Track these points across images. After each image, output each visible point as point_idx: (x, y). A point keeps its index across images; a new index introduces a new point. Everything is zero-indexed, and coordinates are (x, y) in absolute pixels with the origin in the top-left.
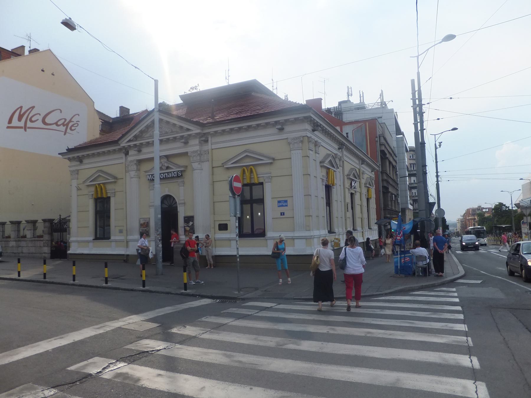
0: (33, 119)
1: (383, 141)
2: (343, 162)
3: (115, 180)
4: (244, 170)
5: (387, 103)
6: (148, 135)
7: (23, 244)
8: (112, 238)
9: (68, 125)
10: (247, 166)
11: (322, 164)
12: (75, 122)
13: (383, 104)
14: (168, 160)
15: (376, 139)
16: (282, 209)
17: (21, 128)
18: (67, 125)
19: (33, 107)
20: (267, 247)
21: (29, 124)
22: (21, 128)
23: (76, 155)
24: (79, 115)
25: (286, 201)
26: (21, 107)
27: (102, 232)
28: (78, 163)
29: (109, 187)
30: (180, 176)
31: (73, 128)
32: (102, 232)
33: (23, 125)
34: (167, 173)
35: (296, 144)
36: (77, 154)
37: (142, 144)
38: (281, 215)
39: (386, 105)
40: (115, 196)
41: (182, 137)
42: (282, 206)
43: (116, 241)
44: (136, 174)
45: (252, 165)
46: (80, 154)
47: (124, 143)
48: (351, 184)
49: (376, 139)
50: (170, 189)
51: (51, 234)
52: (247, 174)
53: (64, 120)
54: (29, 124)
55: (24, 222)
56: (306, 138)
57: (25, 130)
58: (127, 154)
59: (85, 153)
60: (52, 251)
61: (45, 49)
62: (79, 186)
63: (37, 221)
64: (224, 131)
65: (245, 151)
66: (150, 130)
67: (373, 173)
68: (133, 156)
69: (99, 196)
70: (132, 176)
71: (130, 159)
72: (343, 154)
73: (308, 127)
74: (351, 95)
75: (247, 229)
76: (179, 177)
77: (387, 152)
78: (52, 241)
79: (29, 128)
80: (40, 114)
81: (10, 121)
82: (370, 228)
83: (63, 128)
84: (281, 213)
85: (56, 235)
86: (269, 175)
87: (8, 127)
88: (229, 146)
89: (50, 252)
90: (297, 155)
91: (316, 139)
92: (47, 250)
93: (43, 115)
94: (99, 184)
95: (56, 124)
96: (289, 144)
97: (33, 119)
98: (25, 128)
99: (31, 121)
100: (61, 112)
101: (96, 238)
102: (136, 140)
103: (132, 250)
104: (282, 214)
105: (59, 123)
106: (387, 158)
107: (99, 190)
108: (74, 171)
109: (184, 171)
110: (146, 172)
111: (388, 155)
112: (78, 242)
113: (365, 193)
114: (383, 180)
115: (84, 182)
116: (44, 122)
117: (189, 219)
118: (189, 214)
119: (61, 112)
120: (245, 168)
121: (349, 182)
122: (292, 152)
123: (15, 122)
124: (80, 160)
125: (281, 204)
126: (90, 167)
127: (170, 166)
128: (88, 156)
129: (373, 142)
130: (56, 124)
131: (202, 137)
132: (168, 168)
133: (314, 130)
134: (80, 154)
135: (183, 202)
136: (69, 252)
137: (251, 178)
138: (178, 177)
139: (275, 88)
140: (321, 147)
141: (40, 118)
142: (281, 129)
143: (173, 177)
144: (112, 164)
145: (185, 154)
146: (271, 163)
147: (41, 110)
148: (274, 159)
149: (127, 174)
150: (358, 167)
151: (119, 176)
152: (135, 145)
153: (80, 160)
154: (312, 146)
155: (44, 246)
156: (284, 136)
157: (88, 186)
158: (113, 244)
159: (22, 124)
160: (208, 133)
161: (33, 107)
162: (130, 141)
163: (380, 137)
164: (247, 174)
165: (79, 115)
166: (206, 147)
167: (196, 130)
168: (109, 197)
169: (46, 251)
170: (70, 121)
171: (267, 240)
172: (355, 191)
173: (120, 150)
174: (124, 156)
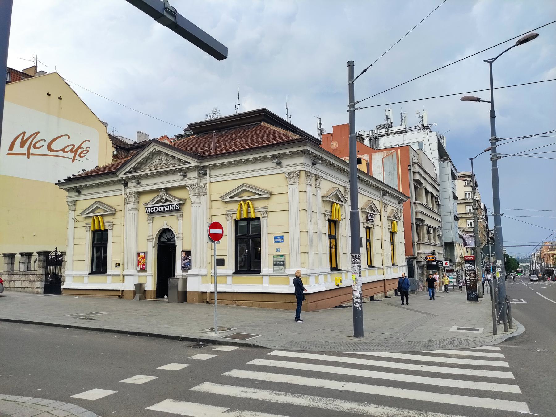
0: (37, 145)
3: (114, 213)
4: (241, 204)
6: (147, 167)
8: (108, 272)
9: (77, 152)
14: (167, 193)
17: (24, 154)
18: (76, 151)
21: (33, 151)
22: (24, 154)
23: (73, 186)
24: (89, 141)
25: (282, 237)
27: (99, 265)
28: (76, 194)
29: (107, 219)
30: (178, 209)
31: (82, 155)
32: (99, 265)
33: (26, 152)
34: (166, 206)
35: (292, 179)
36: (74, 184)
37: (140, 175)
41: (181, 170)
42: (279, 242)
43: (112, 276)
45: (250, 200)
46: (78, 185)
47: (122, 175)
50: (161, 223)
52: (245, 208)
53: (72, 146)
54: (33, 151)
55: (35, 254)
57: (28, 157)
58: (126, 185)
59: (83, 184)
60: (45, 285)
61: (51, 72)
62: (76, 217)
63: (33, 253)
64: (230, 163)
65: (243, 186)
66: (148, 162)
68: (132, 187)
70: (131, 209)
71: (128, 190)
73: (308, 162)
76: (178, 210)
78: (47, 274)
79: (32, 154)
80: (45, 141)
81: (11, 148)
82: (370, 266)
83: (71, 155)
84: (280, 249)
85: (51, 269)
86: (266, 210)
87: (9, 154)
88: (225, 180)
89: (43, 286)
91: (316, 172)
92: (40, 284)
93: (48, 141)
95: (64, 150)
96: (287, 178)
97: (37, 145)
98: (28, 155)
99: (35, 147)
100: (69, 138)
101: (92, 273)
102: (135, 172)
103: (129, 285)
105: (66, 150)
108: (72, 202)
109: (183, 204)
110: (144, 204)
111: (425, 184)
113: (387, 226)
115: (81, 214)
119: (69, 138)
120: (242, 202)
123: (17, 148)
124: (78, 191)
126: (86, 200)
127: (168, 199)
128: (87, 187)
130: (64, 150)
132: (167, 201)
134: (78, 185)
135: (181, 236)
136: (62, 287)
137: (248, 213)
138: (176, 210)
139: (289, 116)
140: (323, 181)
141: (45, 144)
143: (171, 211)
144: (113, 196)
145: (184, 187)
146: (268, 198)
147: (46, 135)
148: (271, 194)
149: (126, 206)
151: (118, 208)
152: (134, 177)
153: (78, 191)
154: (312, 181)
155: (37, 280)
156: (282, 170)
157: (86, 218)
159: (25, 150)
160: (207, 167)
162: (128, 172)
164: (245, 208)
165: (89, 141)
166: (207, 180)
167: (194, 163)
168: (107, 230)
169: (39, 286)
170: (79, 147)
171: (262, 276)
173: (120, 181)
174: (122, 187)
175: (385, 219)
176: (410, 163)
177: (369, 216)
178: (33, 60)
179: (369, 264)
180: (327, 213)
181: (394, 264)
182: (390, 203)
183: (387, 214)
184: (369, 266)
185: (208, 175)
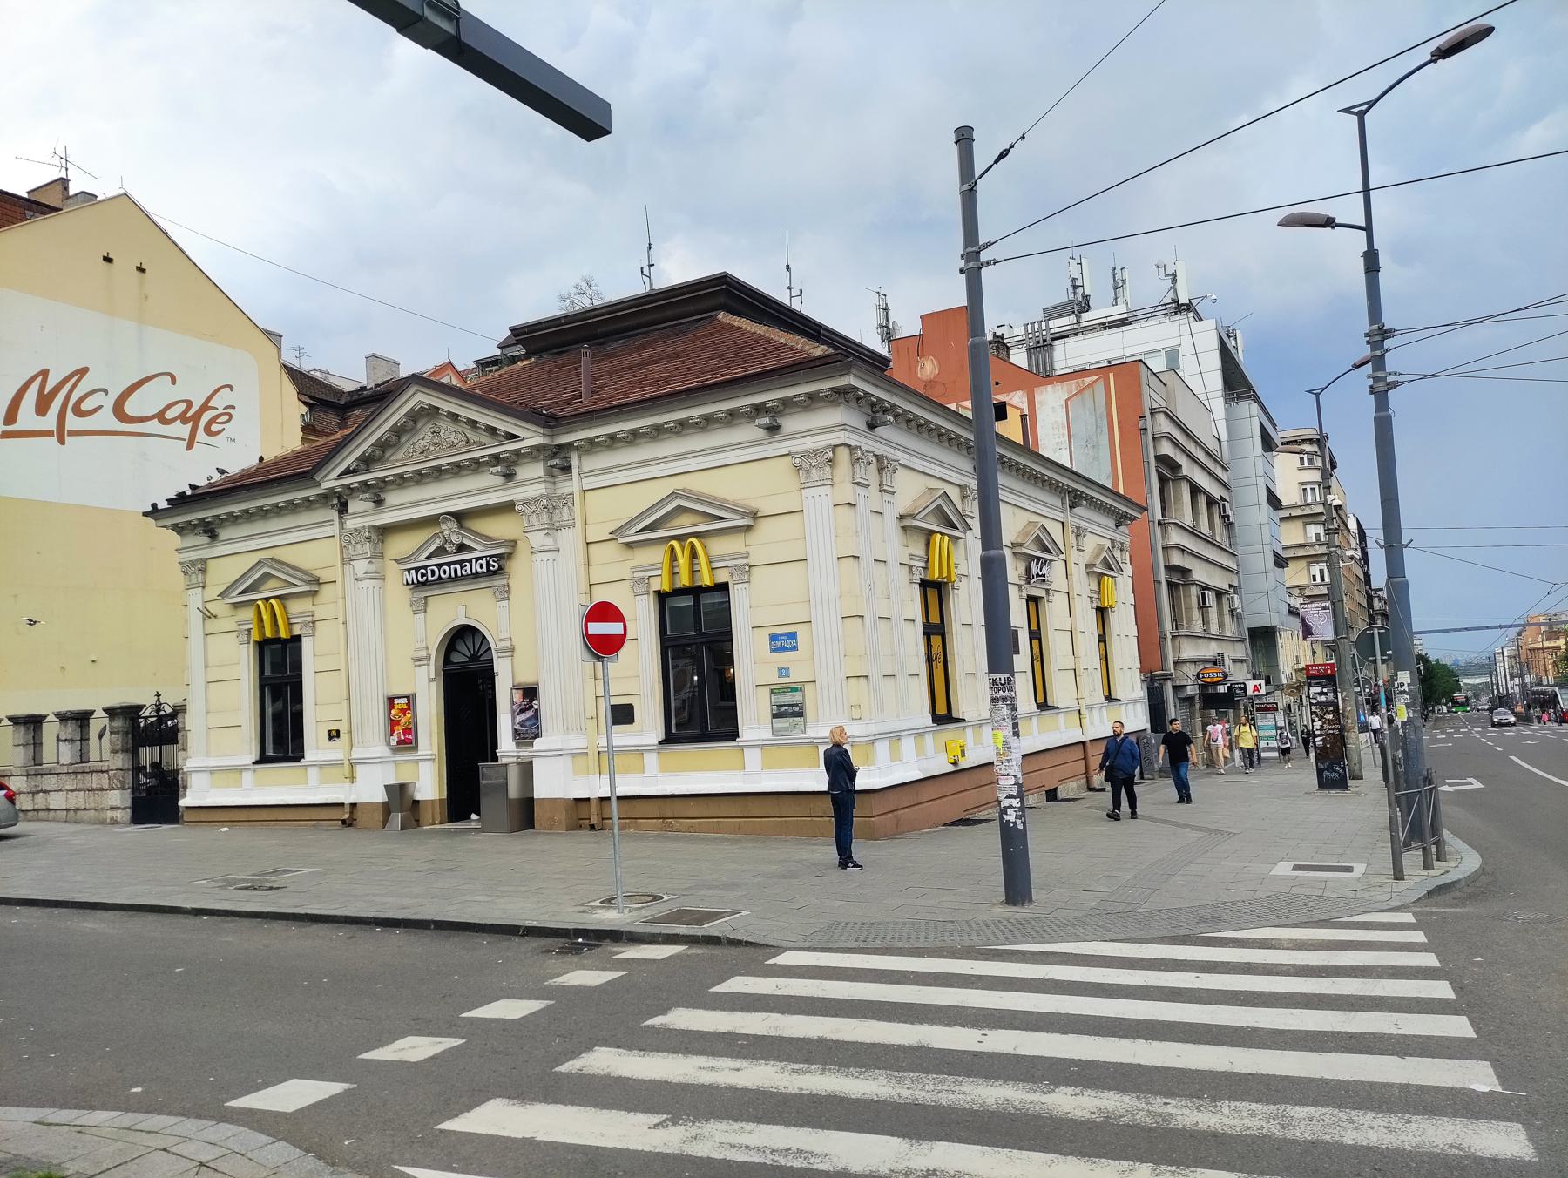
0: (85, 406)
4: (673, 549)
6: (400, 455)
7: (50, 782)
8: (309, 754)
9: (198, 419)
10: (681, 538)
11: (907, 523)
12: (221, 411)
14: (461, 527)
16: (784, 658)
17: (48, 433)
19: (83, 372)
21: (72, 422)
22: (48, 433)
24: (231, 388)
25: (793, 636)
26: (45, 373)
27: (282, 737)
29: (295, 607)
30: (496, 570)
31: (215, 428)
32: (282, 737)
33: (53, 427)
34: (460, 562)
36: (198, 511)
37: (382, 480)
40: (313, 635)
41: (496, 459)
42: (783, 649)
43: (321, 766)
45: (697, 535)
46: (208, 514)
47: (330, 481)
51: (135, 753)
52: (683, 560)
54: (72, 422)
55: (100, 713)
57: (62, 441)
58: (343, 509)
59: (222, 511)
62: (209, 606)
63: (92, 712)
68: (363, 515)
69: (684, 580)
70: (361, 575)
71: (352, 523)
73: (856, 419)
76: (495, 573)
78: (137, 769)
79: (72, 433)
80: (106, 392)
81: (11, 417)
82: (1043, 706)
83: (183, 430)
85: (147, 755)
86: (744, 561)
89: (129, 803)
92: (119, 799)
93: (114, 394)
94: (267, 599)
95: (160, 417)
96: (798, 468)
97: (85, 406)
98: (61, 434)
99: (79, 413)
100: (174, 381)
101: (263, 759)
102: (367, 470)
103: (369, 790)
105: (169, 415)
107: (266, 616)
108: (193, 563)
109: (509, 556)
112: (212, 771)
113: (1086, 593)
116: (119, 411)
118: (526, 678)
119: (174, 381)
120: (674, 543)
123: (27, 418)
124: (210, 530)
127: (466, 541)
128: (233, 519)
130: (160, 417)
131: (552, 457)
132: (462, 548)
133: (872, 427)
134: (208, 514)
135: (507, 644)
136: (182, 803)
138: (491, 573)
139: (795, 292)
140: (901, 472)
141: (108, 402)
142: (773, 429)
143: (476, 575)
145: (507, 508)
146: (748, 528)
147: (109, 377)
148: (755, 516)
151: (324, 575)
152: (365, 486)
155: (111, 788)
156: (783, 447)
157: (236, 605)
158: (313, 773)
159: (49, 422)
160: (569, 446)
161: (83, 372)
162: (348, 472)
164: (683, 560)
166: (572, 485)
167: (531, 437)
168: (298, 638)
169: (118, 803)
170: (206, 407)
173: (325, 498)
174: (334, 514)
175: (1078, 573)
177: (1033, 564)
178: (57, 161)
179: (1041, 700)
181: (1109, 698)
182: (1091, 527)
183: (1085, 557)
184: (1039, 706)
185: (575, 471)
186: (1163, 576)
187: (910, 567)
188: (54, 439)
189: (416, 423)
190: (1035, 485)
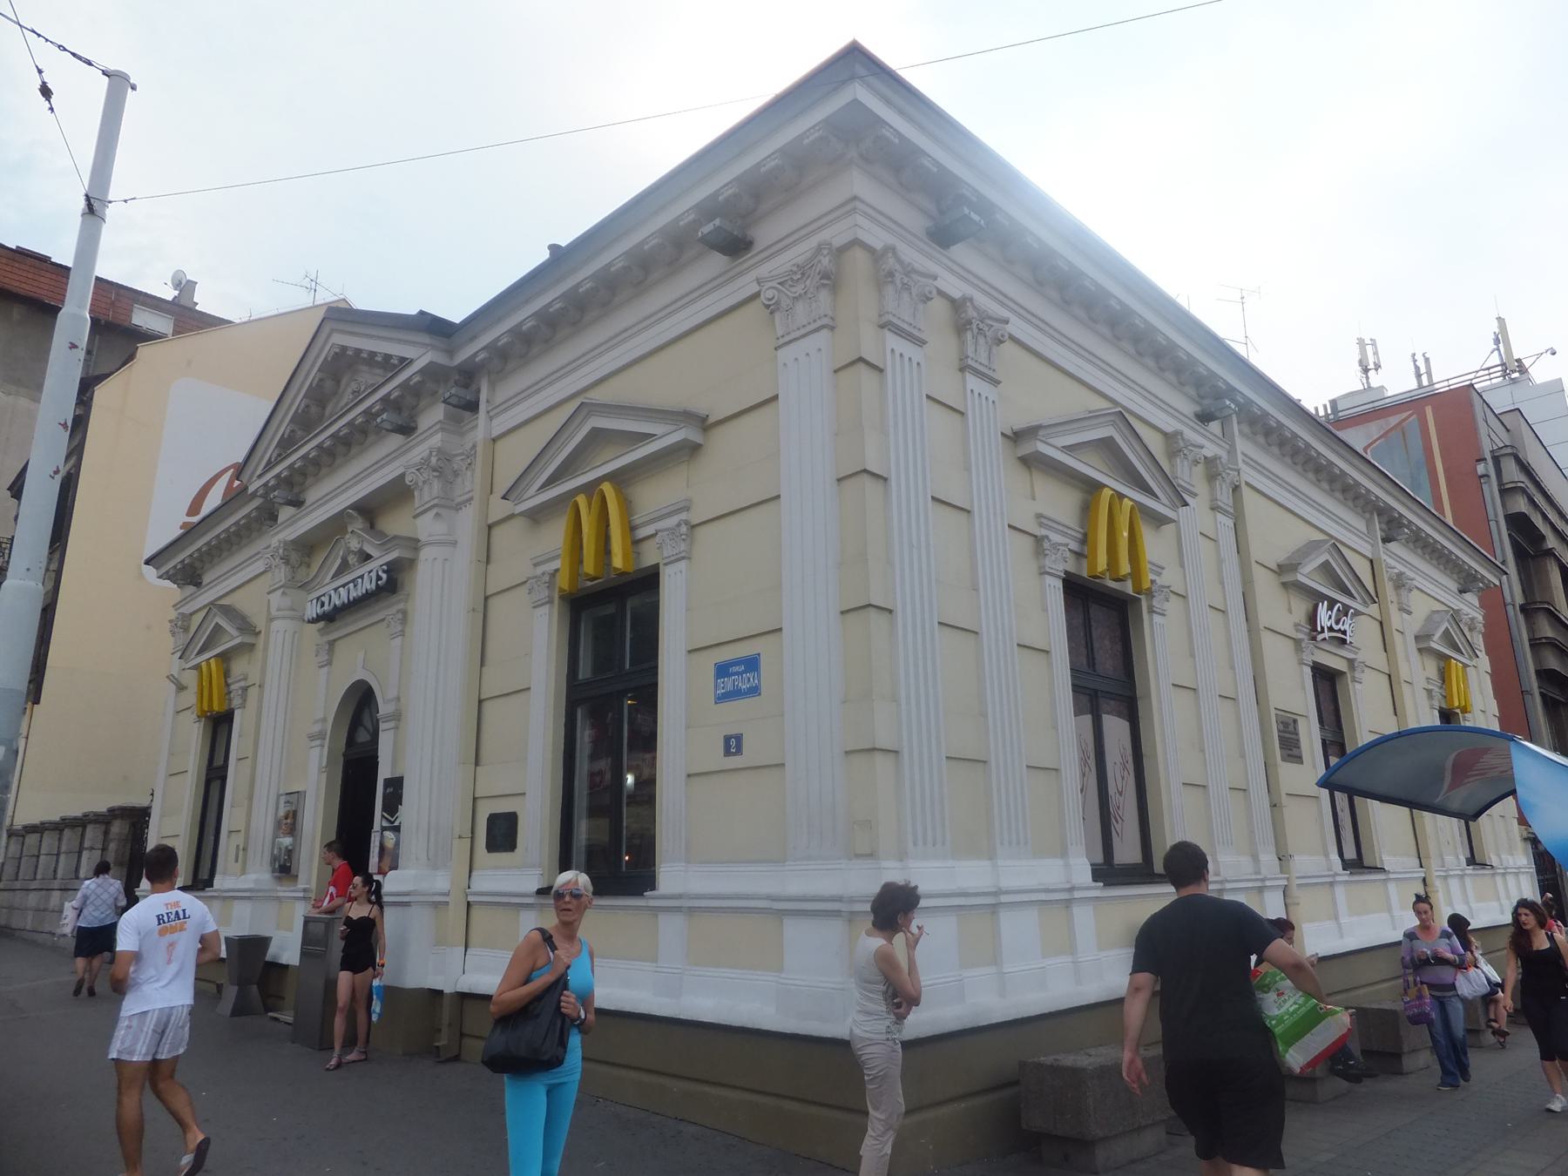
1: (1512, 473)
2: (1236, 489)
5: (1527, 363)
8: (671, 876)
13: (1514, 370)
15: (1481, 469)
16: (735, 716)
20: (654, 959)
25: (752, 664)
38: (727, 753)
39: (1522, 369)
42: (735, 694)
44: (287, 602)
48: (1312, 618)
49: (1481, 469)
56: (859, 255)
67: (1468, 596)
72: (1232, 451)
74: (1377, 367)
75: (1127, 851)
77: (1538, 521)
84: (727, 739)
86: (683, 516)
90: (804, 373)
104: (733, 745)
106: (1550, 553)
113: (1420, 683)
114: (1536, 644)
117: (395, 785)
121: (1300, 608)
122: (786, 354)
125: (729, 683)
129: (1464, 484)
148: (705, 424)
150: (1366, 549)
162: (270, 465)
163: (1497, 461)
172: (1351, 662)
175: (1405, 647)
176: (1479, 448)
177: (1323, 609)
178: (306, 282)
179: (1350, 853)
180: (1055, 538)
181: (1472, 861)
182: (1419, 581)
183: (1413, 624)
184: (1346, 865)
185: (483, 406)
186: (1533, 683)
187: (1039, 540)
188: (1475, 924)
189: (338, 382)
190: (1317, 483)
